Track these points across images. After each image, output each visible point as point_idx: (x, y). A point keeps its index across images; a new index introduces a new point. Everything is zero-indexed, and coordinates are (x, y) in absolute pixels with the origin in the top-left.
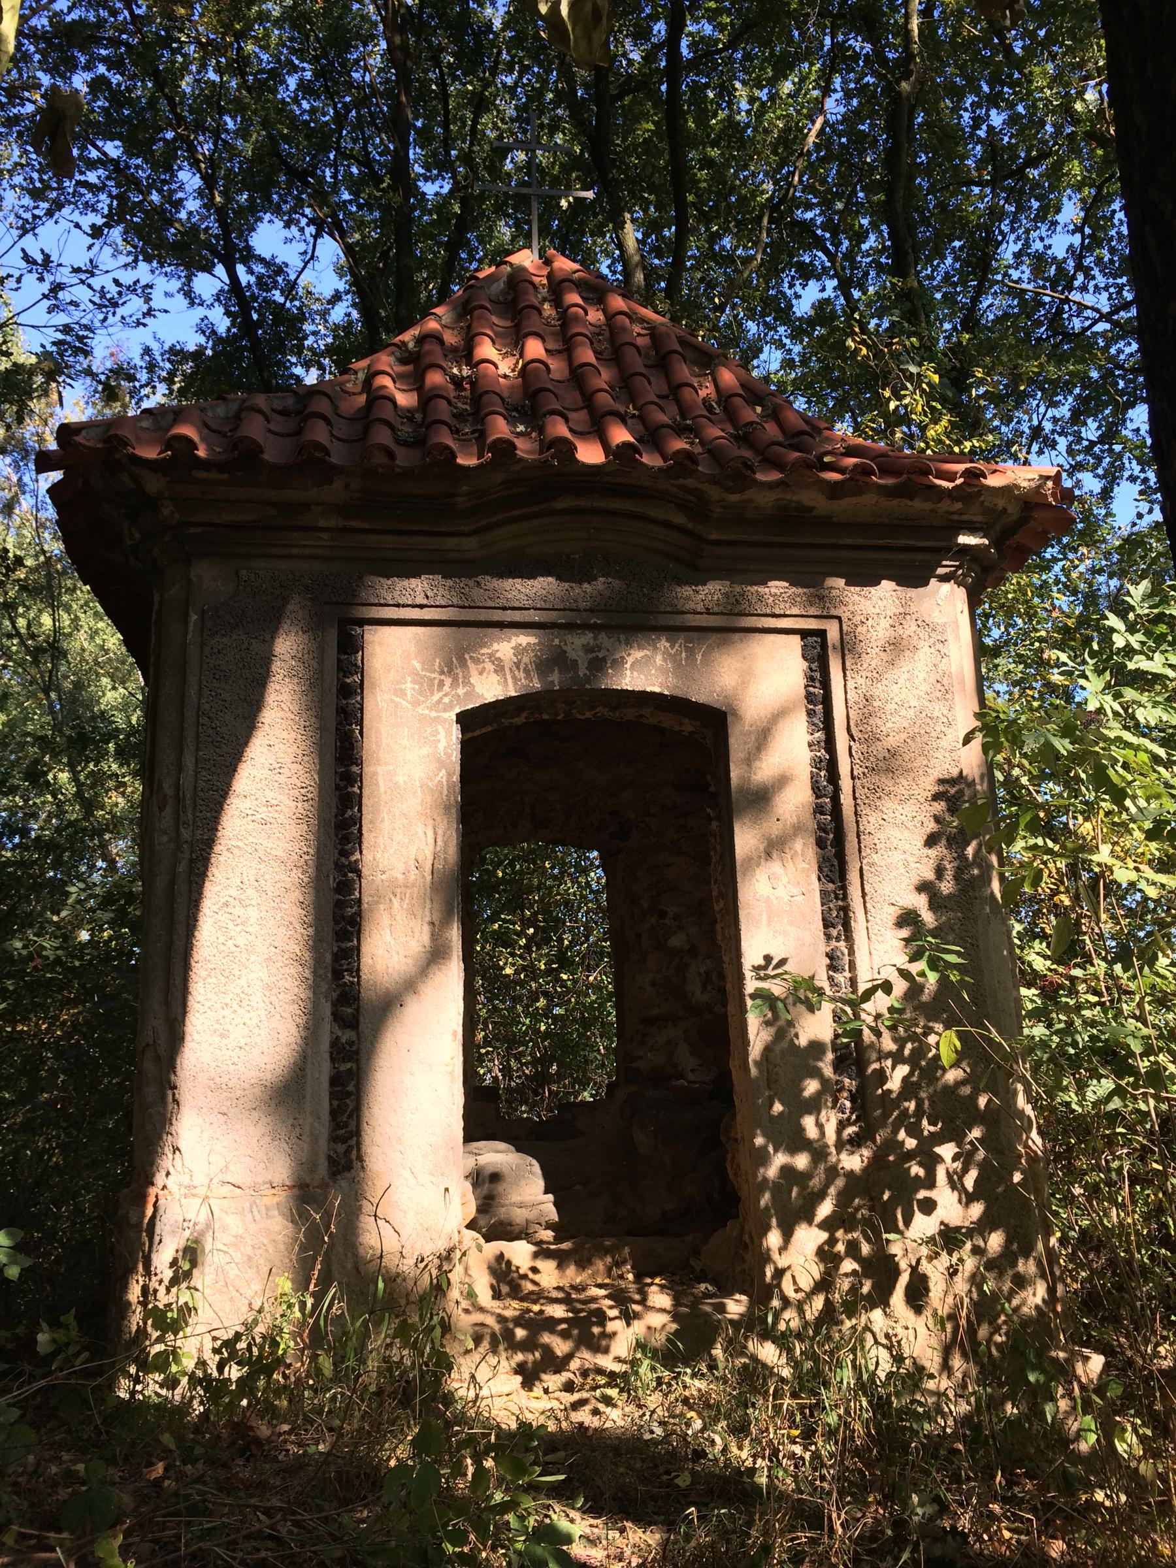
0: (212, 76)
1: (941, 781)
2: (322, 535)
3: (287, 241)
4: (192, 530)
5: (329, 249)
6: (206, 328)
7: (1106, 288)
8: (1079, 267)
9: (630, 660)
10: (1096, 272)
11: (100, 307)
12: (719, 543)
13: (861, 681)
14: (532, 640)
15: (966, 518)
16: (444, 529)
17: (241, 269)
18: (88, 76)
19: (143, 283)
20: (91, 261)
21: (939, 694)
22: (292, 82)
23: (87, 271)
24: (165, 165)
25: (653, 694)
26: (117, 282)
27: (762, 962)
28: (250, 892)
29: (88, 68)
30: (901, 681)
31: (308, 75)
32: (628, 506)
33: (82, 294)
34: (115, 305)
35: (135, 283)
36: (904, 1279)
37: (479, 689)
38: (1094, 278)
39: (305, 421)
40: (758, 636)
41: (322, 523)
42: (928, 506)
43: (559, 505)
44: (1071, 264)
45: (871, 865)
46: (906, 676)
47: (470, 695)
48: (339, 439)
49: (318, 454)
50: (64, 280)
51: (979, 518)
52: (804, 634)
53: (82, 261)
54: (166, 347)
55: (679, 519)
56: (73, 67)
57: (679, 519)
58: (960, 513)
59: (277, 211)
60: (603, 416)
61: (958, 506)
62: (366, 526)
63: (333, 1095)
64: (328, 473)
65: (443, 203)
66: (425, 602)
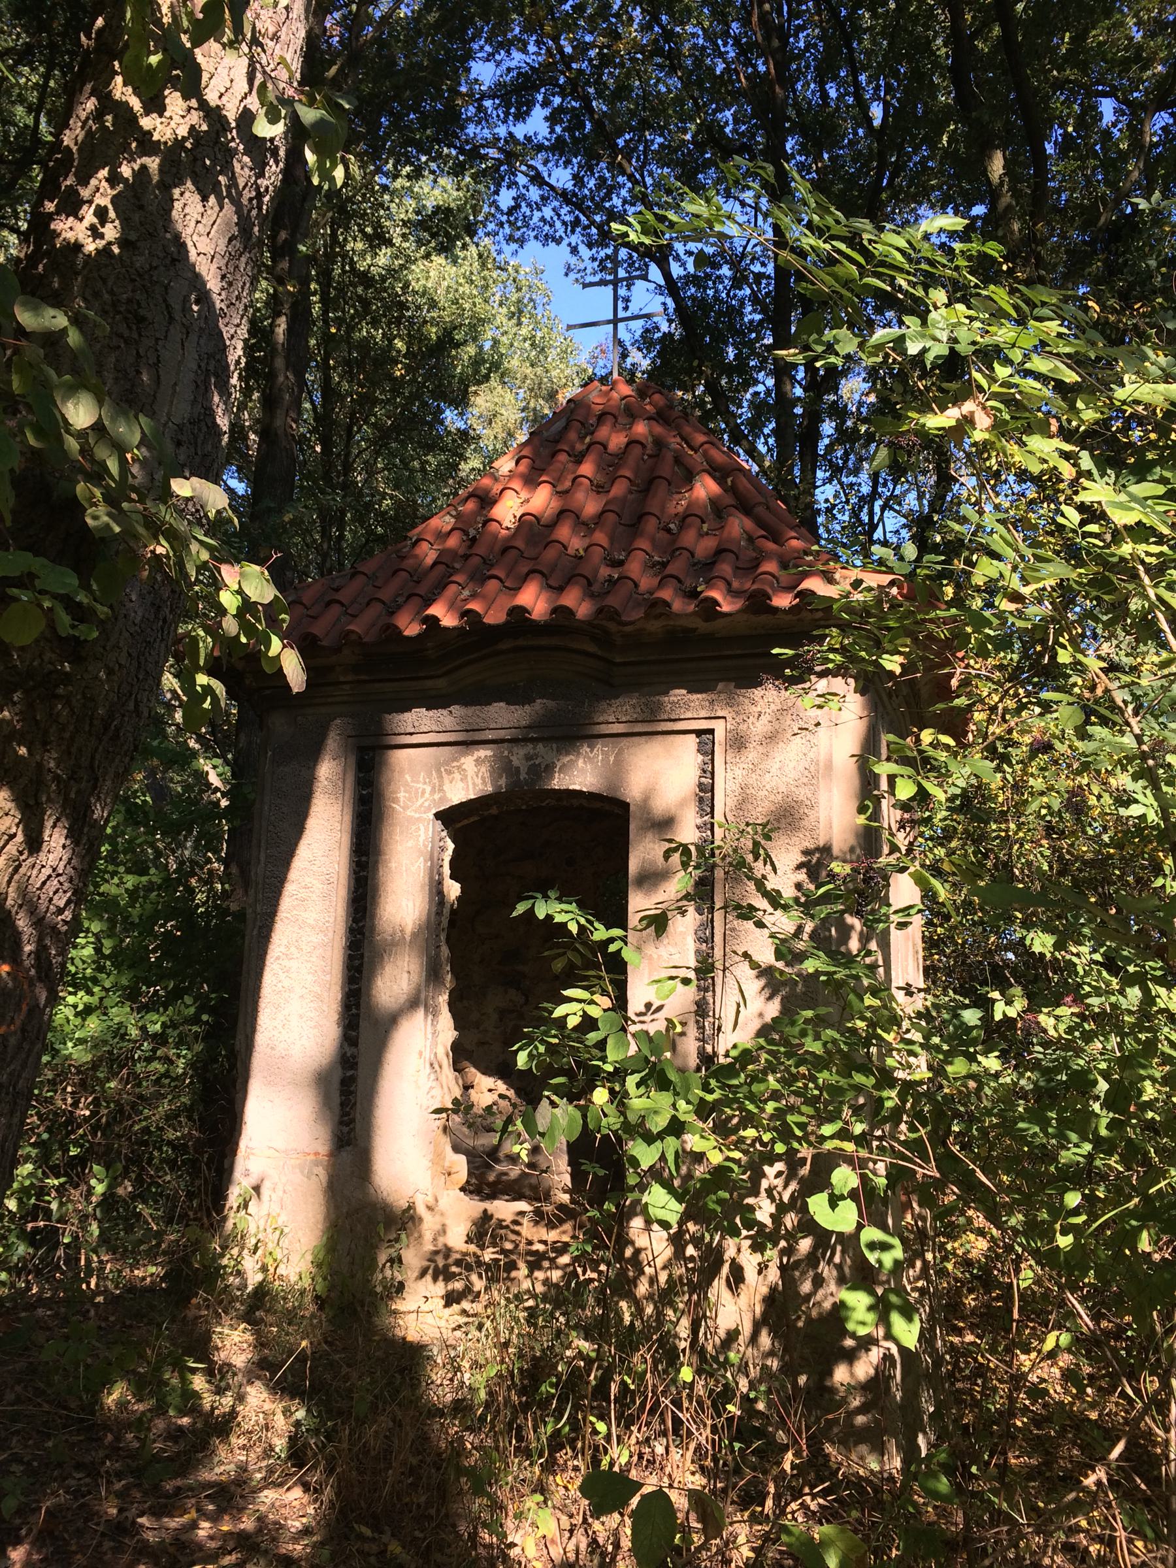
1: (806, 852)
4: (268, 692)
9: (559, 765)
12: (624, 664)
13: (738, 772)
14: (489, 753)
18: (547, 112)
21: (805, 780)
25: (574, 791)
27: (643, 1010)
28: (293, 949)
30: (773, 770)
36: (725, 1269)
37: (449, 795)
40: (660, 737)
41: (342, 679)
43: (503, 646)
45: (733, 930)
46: (778, 765)
47: (443, 799)
52: (699, 733)
55: (592, 648)
57: (592, 648)
63: (342, 1093)
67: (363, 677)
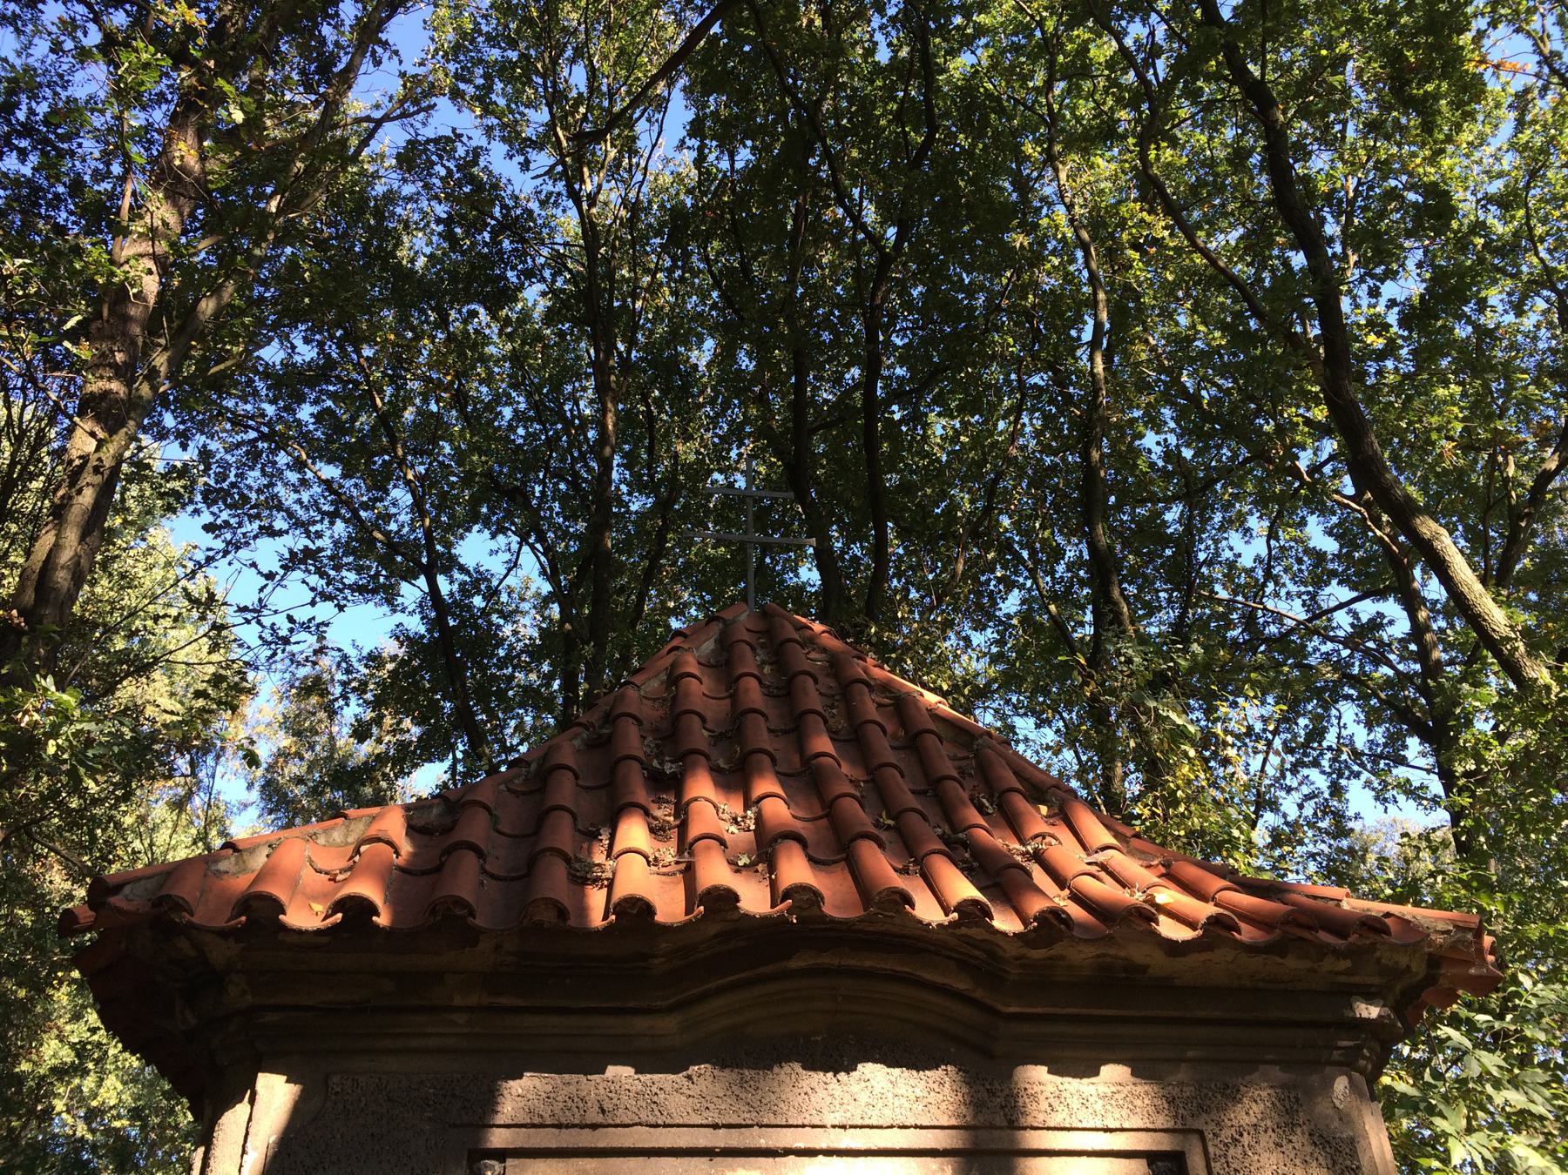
0: (434, 407)
2: (455, 1017)
3: (493, 553)
4: (271, 1017)
5: (530, 563)
6: (401, 635)
7: (1299, 595)
8: (1268, 575)
10: (1286, 579)
11: (266, 643)
15: (1353, 980)
16: (632, 1004)
17: (442, 581)
18: (315, 409)
19: (318, 620)
20: (260, 600)
22: (507, 412)
23: (254, 611)
24: (380, 484)
26: (291, 619)
29: (316, 402)
31: (522, 406)
32: (890, 964)
33: (250, 634)
34: (286, 641)
35: (310, 621)
38: (1284, 585)
39: (449, 851)
42: (1306, 964)
43: (795, 964)
44: (1260, 573)
48: (492, 876)
49: (459, 912)
50: (230, 621)
51: (1376, 980)
53: (250, 600)
54: (365, 653)
55: (961, 984)
56: (301, 399)
57: (961, 984)
58: (1347, 972)
59: (486, 523)
60: (853, 840)
61: (1345, 964)
62: (520, 1002)
64: (471, 936)
65: (642, 516)
66: (600, 1119)
67: (505, 1001)
